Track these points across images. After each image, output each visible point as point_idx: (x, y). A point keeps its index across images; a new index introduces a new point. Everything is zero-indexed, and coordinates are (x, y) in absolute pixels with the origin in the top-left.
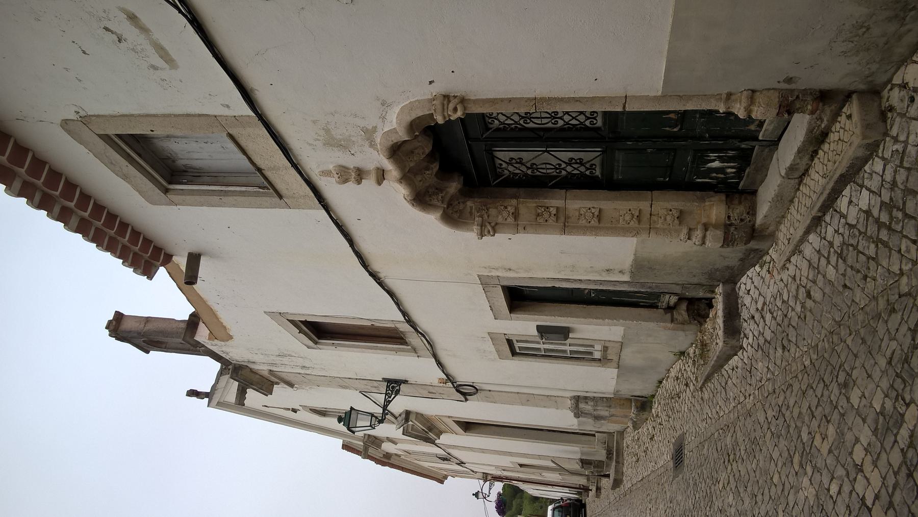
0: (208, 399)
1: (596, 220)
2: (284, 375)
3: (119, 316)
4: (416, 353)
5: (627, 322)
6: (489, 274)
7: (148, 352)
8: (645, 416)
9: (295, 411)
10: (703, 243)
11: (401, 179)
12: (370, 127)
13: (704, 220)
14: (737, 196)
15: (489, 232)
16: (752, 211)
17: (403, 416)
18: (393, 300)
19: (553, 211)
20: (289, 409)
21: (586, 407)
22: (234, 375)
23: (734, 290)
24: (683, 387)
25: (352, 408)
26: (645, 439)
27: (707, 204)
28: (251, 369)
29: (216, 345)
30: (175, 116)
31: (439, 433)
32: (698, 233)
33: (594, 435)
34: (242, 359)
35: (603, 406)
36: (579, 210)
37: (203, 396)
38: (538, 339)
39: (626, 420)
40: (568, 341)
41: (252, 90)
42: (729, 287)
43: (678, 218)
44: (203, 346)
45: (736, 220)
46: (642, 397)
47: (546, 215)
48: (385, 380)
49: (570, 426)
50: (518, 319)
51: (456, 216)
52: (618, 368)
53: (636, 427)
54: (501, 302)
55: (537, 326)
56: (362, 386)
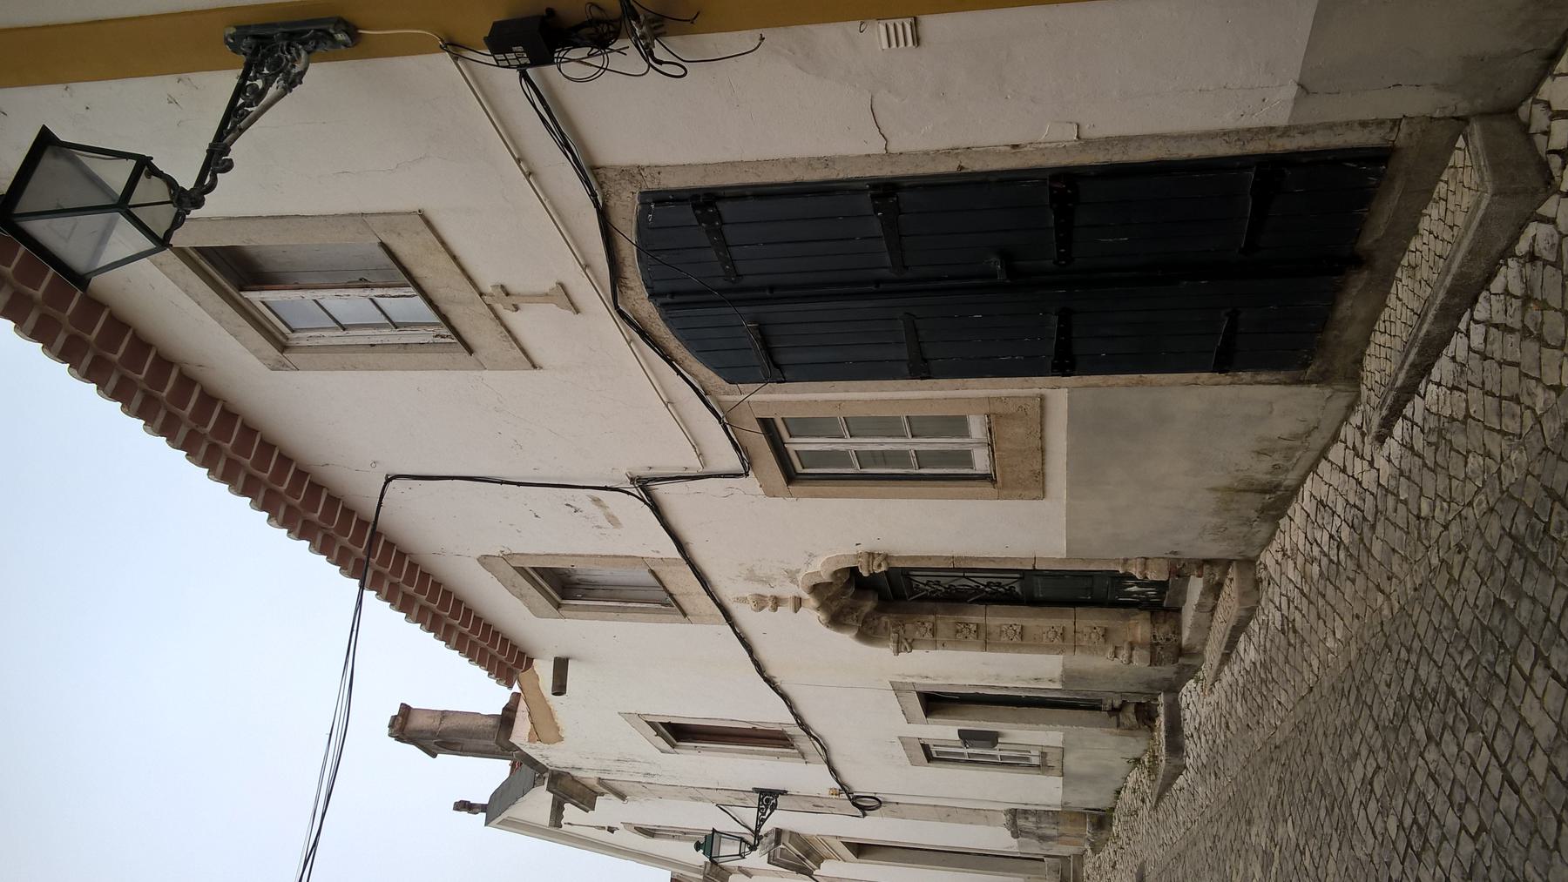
0: (484, 814)
2: (616, 785)
3: (405, 710)
4: (804, 758)
5: (1066, 727)
6: (904, 681)
7: (434, 756)
8: (1104, 836)
9: (611, 830)
10: (1131, 662)
13: (1130, 639)
14: (1162, 613)
15: (906, 649)
16: (1178, 630)
17: (773, 837)
18: (786, 703)
20: (603, 828)
21: (1027, 824)
22: (552, 786)
23: (1176, 700)
24: (1140, 803)
25: (714, 830)
26: (1107, 867)
27: (1132, 622)
28: (572, 777)
29: (536, 748)
30: (602, 556)
31: (819, 861)
32: (1124, 653)
33: (1043, 860)
34: (565, 765)
35: (1048, 823)
36: (1000, 626)
37: (478, 810)
38: (960, 744)
39: (1082, 841)
40: (998, 746)
41: (687, 543)
42: (1171, 697)
43: (1103, 636)
44: (519, 749)
46: (1099, 810)
47: (966, 631)
48: (756, 790)
49: (1007, 848)
50: (935, 723)
51: (870, 632)
52: (1063, 776)
53: (1095, 850)
54: (916, 707)
55: (959, 731)
56: (722, 798)
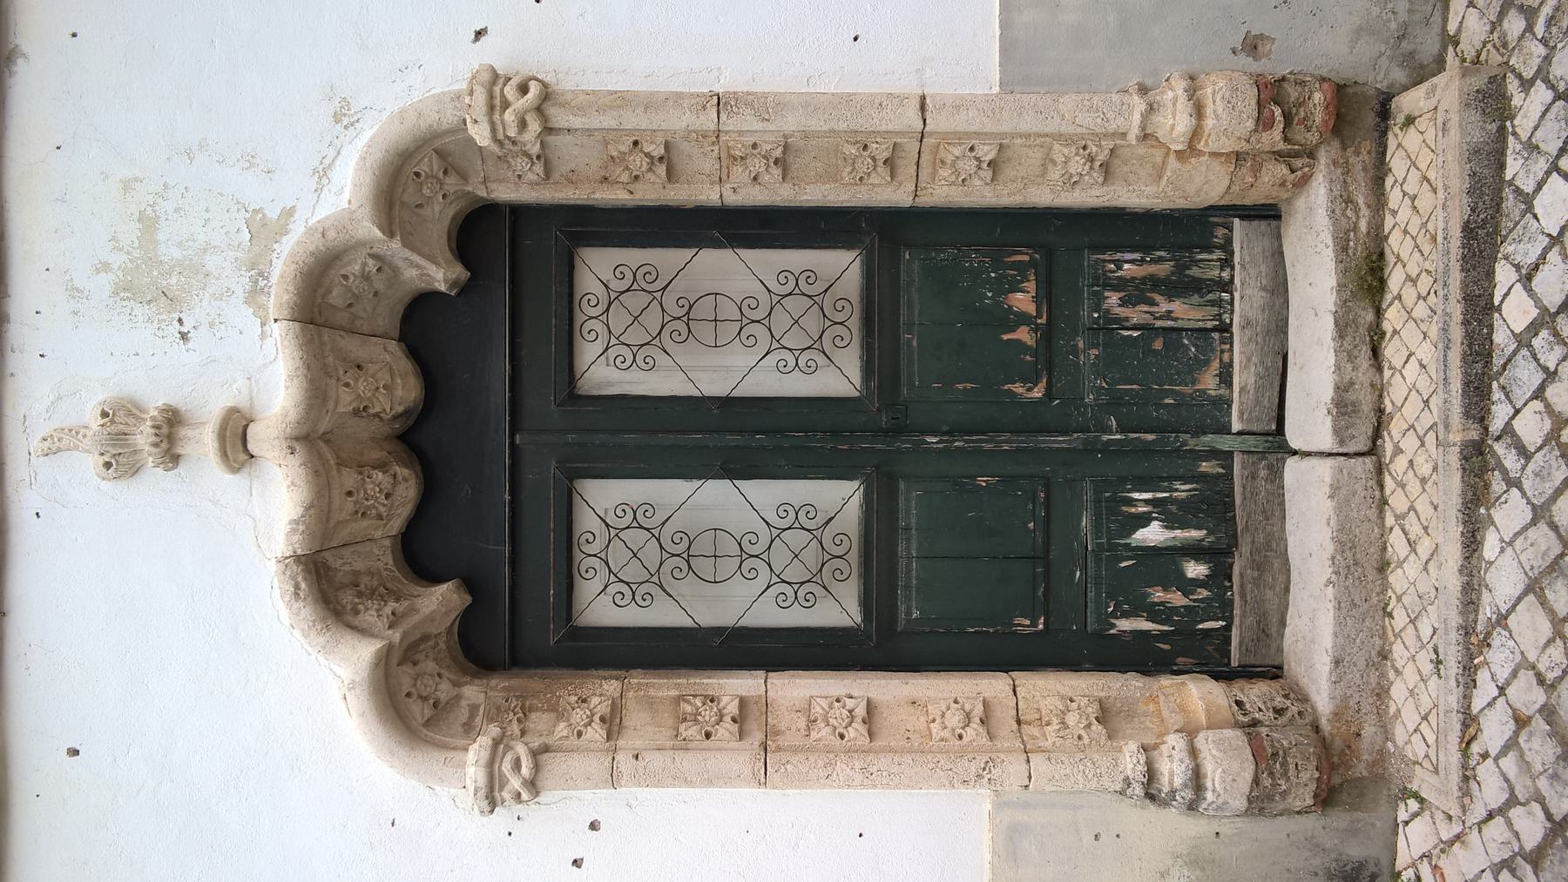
1: (863, 729)
11: (297, 439)
12: (273, 213)
19: (732, 708)
45: (1260, 710)
51: (419, 711)
